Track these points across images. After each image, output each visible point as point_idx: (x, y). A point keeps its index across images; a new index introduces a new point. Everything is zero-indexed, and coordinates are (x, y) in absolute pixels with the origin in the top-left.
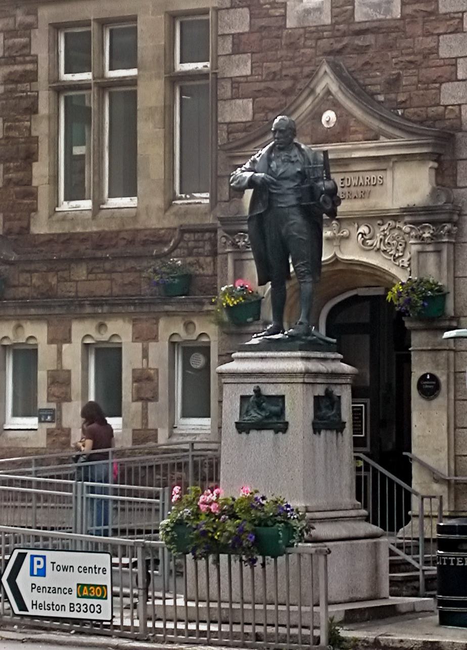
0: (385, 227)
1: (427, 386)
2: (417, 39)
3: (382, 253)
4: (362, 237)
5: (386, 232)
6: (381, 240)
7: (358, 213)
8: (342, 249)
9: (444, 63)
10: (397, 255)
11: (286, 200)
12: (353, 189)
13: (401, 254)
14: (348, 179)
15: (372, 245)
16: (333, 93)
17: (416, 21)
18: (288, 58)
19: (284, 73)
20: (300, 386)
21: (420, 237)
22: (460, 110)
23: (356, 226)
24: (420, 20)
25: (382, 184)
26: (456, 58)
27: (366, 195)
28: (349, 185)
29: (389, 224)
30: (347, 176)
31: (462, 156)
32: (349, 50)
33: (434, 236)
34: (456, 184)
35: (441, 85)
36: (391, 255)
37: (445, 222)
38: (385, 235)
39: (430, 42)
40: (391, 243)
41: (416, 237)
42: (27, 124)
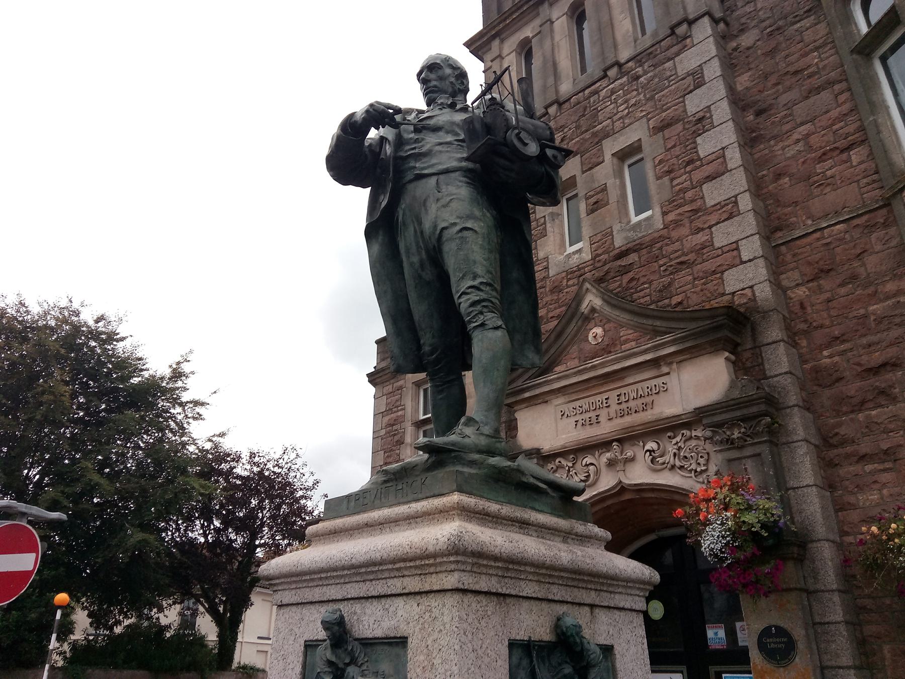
0: (678, 439)
1: (773, 646)
2: (684, 240)
3: (678, 471)
4: (650, 455)
5: (679, 444)
6: (675, 455)
7: (640, 428)
8: (628, 475)
9: (723, 252)
10: (699, 470)
11: (434, 161)
12: (632, 404)
13: (703, 468)
14: (625, 394)
15: (664, 463)
16: (598, 308)
17: (681, 225)
18: (553, 302)
19: (551, 315)
20: (451, 600)
21: (728, 440)
22: (753, 292)
23: (641, 444)
24: (686, 221)
25: (666, 390)
26: (737, 242)
27: (649, 407)
28: (627, 399)
29: (683, 434)
30: (623, 391)
31: (765, 341)
32: (612, 274)
33: (748, 436)
34: (764, 374)
35: (723, 274)
36: (691, 471)
37: (761, 416)
38: (679, 449)
39: (701, 238)
40: (688, 456)
41: (721, 442)
42: (398, 452)
